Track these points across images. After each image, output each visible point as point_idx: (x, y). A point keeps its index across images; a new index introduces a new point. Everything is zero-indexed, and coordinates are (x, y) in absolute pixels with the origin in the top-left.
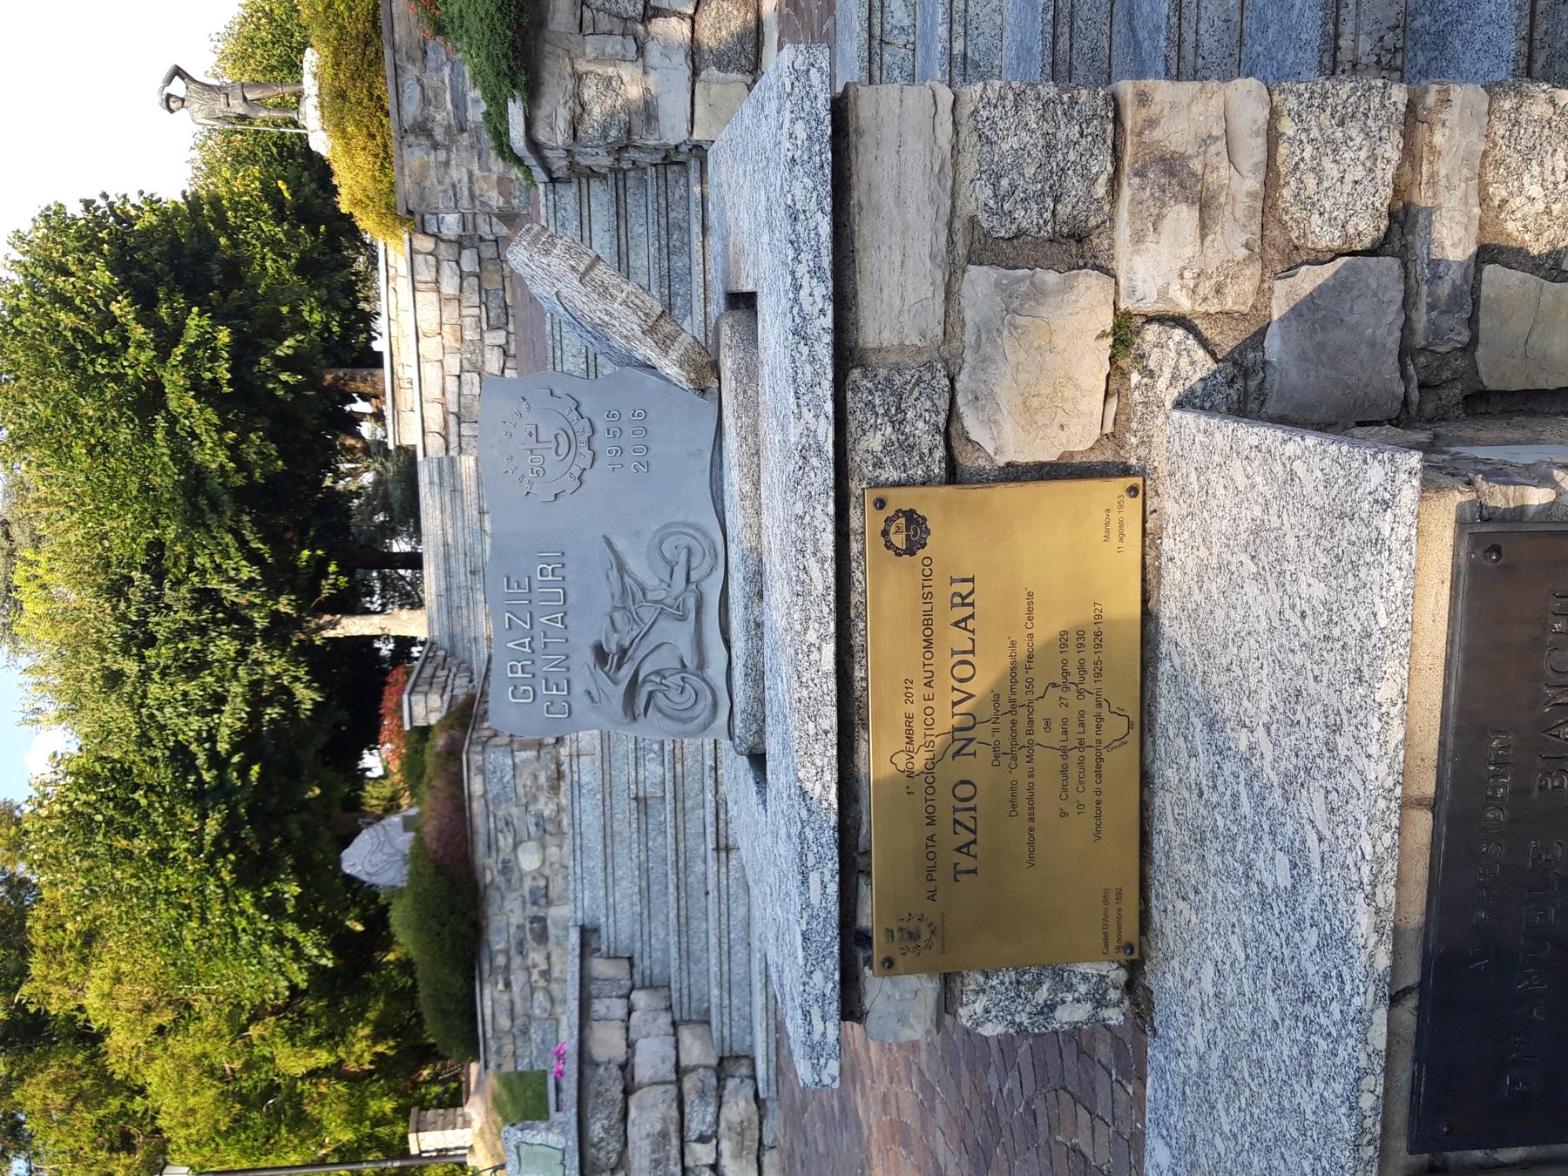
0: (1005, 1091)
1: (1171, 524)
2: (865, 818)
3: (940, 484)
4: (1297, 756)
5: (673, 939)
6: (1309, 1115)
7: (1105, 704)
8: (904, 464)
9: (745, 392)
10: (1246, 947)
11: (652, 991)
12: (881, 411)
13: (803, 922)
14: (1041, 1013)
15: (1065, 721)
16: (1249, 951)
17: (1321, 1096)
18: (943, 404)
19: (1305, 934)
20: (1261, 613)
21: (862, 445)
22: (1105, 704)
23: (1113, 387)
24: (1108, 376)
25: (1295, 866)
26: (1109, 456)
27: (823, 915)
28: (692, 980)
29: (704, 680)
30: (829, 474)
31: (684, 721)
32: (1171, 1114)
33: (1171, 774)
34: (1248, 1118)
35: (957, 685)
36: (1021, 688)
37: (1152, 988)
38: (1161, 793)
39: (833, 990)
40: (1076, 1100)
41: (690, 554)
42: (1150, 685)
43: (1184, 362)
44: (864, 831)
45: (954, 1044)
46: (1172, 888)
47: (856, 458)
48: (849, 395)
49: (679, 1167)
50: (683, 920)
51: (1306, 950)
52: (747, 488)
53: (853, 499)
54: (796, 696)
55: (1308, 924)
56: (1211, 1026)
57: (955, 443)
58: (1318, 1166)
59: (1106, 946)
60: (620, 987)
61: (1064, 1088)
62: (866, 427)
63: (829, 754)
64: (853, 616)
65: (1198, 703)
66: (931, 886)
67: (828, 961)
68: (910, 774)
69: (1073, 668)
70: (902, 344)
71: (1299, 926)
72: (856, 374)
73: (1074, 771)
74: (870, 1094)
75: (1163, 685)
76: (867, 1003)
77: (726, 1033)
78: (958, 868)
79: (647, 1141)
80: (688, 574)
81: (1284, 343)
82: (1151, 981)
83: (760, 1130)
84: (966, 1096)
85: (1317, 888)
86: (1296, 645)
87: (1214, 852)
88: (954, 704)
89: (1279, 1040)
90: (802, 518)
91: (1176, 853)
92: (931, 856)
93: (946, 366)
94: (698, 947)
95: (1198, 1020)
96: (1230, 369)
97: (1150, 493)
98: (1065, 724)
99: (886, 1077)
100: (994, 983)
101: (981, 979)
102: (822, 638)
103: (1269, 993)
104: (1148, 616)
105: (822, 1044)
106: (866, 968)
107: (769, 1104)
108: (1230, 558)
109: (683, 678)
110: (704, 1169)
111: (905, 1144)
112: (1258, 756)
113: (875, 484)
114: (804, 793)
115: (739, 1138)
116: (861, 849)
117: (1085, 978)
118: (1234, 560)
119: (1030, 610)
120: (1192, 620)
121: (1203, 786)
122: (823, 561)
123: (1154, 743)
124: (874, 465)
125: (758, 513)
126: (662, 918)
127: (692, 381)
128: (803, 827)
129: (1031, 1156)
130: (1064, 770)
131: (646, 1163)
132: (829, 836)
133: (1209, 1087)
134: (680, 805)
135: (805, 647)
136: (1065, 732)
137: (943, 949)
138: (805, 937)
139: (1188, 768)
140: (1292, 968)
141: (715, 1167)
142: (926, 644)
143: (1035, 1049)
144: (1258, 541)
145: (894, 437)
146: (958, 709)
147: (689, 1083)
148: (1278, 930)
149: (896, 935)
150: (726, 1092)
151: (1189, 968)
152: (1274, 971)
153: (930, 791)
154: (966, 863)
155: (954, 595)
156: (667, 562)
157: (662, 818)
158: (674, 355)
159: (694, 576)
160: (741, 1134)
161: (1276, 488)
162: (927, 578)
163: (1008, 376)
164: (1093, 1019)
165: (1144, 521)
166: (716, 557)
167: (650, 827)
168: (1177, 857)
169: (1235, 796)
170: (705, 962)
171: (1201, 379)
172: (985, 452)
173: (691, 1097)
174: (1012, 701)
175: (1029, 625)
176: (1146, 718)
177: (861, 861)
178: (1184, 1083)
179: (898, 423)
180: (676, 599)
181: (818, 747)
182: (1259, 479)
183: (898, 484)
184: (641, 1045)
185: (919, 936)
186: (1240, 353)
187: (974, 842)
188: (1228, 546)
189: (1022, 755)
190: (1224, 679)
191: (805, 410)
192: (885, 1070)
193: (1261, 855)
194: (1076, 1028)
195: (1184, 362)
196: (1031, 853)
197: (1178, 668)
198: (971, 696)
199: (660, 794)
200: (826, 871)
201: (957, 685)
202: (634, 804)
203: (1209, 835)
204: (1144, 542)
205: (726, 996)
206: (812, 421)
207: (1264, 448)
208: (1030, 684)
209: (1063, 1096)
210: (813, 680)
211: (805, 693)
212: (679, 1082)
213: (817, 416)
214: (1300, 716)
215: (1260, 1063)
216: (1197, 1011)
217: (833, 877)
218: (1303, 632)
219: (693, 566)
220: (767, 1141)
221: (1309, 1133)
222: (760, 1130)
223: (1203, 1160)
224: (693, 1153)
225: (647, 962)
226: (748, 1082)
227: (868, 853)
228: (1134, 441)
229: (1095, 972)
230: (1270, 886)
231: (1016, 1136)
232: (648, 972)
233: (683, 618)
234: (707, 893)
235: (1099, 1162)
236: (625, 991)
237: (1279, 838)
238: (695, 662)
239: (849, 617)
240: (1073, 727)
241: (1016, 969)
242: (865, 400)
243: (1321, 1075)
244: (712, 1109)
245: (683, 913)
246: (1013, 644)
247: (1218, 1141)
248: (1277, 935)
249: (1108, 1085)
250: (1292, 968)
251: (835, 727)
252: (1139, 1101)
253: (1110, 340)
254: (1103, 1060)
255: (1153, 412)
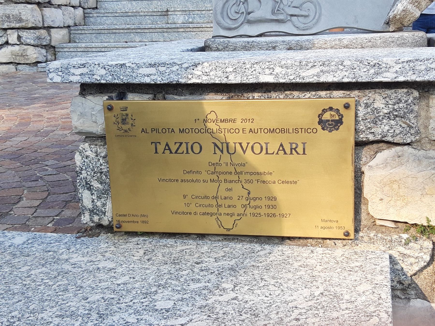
0: (47, 168)
1: (330, 252)
2: (182, 97)
3: (355, 138)
4: (224, 314)
5: (106, 27)
6: (41, 316)
7: (239, 218)
8: (366, 119)
9: (393, 42)
10: (124, 284)
11: (83, 17)
12: (396, 107)
13: (130, 65)
14: (87, 183)
15: (231, 198)
16: (122, 285)
17: (51, 322)
18: (397, 140)
19: (133, 316)
20: (294, 297)
21: (377, 97)
22: (239, 218)
23: (400, 225)
24: (406, 223)
25: (167, 311)
26: (364, 222)
27: (134, 75)
28: (88, 35)
29: (242, 24)
30: (364, 79)
31: (222, 13)
32: (39, 245)
33: (205, 248)
34: (38, 283)
35: (250, 145)
36: (248, 177)
37: (100, 237)
38: (195, 243)
39: (96, 79)
40: (44, 200)
41: (306, 16)
42: (248, 240)
43: (412, 260)
44: (176, 97)
45: (67, 146)
46: (149, 247)
47: (371, 94)
48: (405, 90)
49: (7, 27)
50: (114, 31)
51: (125, 316)
52: (345, 42)
53: (348, 93)
54: (246, 62)
55: (139, 317)
56: (83, 266)
57: (375, 146)
58: (15, 320)
59: (120, 216)
60: (85, 3)
61: (49, 194)
62: (387, 99)
63: (216, 78)
64: (286, 92)
65: (243, 263)
66: (149, 130)
67: (110, 77)
68: (205, 121)
69: (258, 203)
70: (431, 118)
71: (137, 312)
72: (416, 94)
73: (206, 202)
74: (42, 109)
75: (248, 246)
76: (90, 97)
77: (65, 50)
78: (158, 144)
79: (18, 13)
80: (295, 16)
81: (419, 309)
82: (103, 236)
83: (24, 64)
84: (43, 150)
85: (157, 323)
86: (281, 315)
87: (170, 269)
88: (240, 144)
89: (78, 300)
90: (342, 64)
91: (167, 250)
92: (164, 131)
93: (417, 141)
94: (103, 38)
95: (86, 259)
96: (407, 283)
97: (344, 242)
98: (230, 198)
99: (50, 116)
100: (101, 161)
101: (103, 155)
102: (277, 76)
103: (102, 296)
104: (282, 239)
105: (69, 74)
106: (107, 97)
107: (35, 68)
108: (320, 281)
109: (243, 13)
110: (6, 38)
111: (20, 124)
112: (220, 293)
113: (357, 104)
114: (196, 65)
115: (20, 54)
116: (167, 96)
117: (104, 205)
118: (318, 284)
119: (287, 182)
120: (284, 261)
121: (201, 265)
122: (318, 76)
123: (219, 240)
124: (366, 104)
125: (332, 48)
126: (115, 22)
127: (395, 17)
128: (178, 65)
129: (17, 179)
130: (206, 197)
131: (8, 12)
132: (174, 79)
133: (53, 264)
134: (165, 30)
135: (272, 66)
136: (225, 198)
137: (118, 136)
138: (122, 65)
139: (209, 257)
140: (115, 308)
141: (7, 43)
142: (272, 130)
143: (67, 181)
144: (331, 297)
145: (381, 114)
146: (238, 146)
147: (43, 32)
148: (133, 301)
149: (124, 113)
150: (40, 49)
151: (111, 255)
152: (113, 298)
153: (197, 131)
154: (161, 148)
155: (297, 145)
156: (301, 5)
157: (159, 23)
158: (410, 7)
159: (294, 18)
160: (22, 55)
161: (362, 307)
162: (306, 131)
163: (410, 173)
164: (84, 208)
165: (330, 239)
166: (304, 30)
167: (155, 17)
168: (165, 250)
169: (199, 281)
170: (96, 41)
171: (402, 268)
172: (370, 161)
173: (38, 33)
174: (241, 173)
175: (280, 182)
176: (231, 237)
177: (160, 96)
178: (54, 252)
179: (388, 116)
180: (283, 10)
181: (220, 73)
182: (364, 298)
183: (356, 116)
184: (59, 11)
185: (123, 124)
186: (415, 288)
187: (171, 152)
188: (325, 281)
189: (215, 177)
190: (257, 277)
191: (400, 66)
192: (53, 116)
193: (170, 293)
194: (80, 200)
195: (412, 260)
196: (166, 181)
197: (258, 254)
198: (244, 152)
199: (170, 22)
200: (156, 77)
201: (250, 145)
202: (165, 10)
203: (178, 267)
204: (319, 238)
205: (81, 50)
206: (394, 70)
207: (381, 301)
208: (250, 182)
209: (45, 194)
210: (255, 70)
211: (248, 66)
212: (44, 28)
213: (396, 72)
214: (244, 316)
215: (66, 290)
216: (90, 259)
217: (153, 80)
218: (288, 319)
219: (299, 18)
220: (20, 67)
221: (32, 315)
222: (24, 64)
223: (17, 260)
224: (13, 33)
225: (95, 15)
226: (45, 59)
227: (165, 99)
228: (372, 235)
229: (107, 210)
230: (156, 297)
231: (26, 172)
232: (91, 15)
233: (273, 13)
234: (126, 42)
235: (15, 210)
236: (82, 5)
237: (181, 303)
238: (251, 19)
239: (285, 90)
240: (228, 202)
241: (108, 171)
242: (402, 99)
243: (62, 322)
244: (32, 42)
245: (117, 31)
246: (271, 174)
247: (27, 268)
248: (131, 301)
249: (51, 215)
250: (115, 308)
251: (230, 82)
252: (45, 229)
253: (426, 224)
254: (63, 213)
255: (386, 244)
